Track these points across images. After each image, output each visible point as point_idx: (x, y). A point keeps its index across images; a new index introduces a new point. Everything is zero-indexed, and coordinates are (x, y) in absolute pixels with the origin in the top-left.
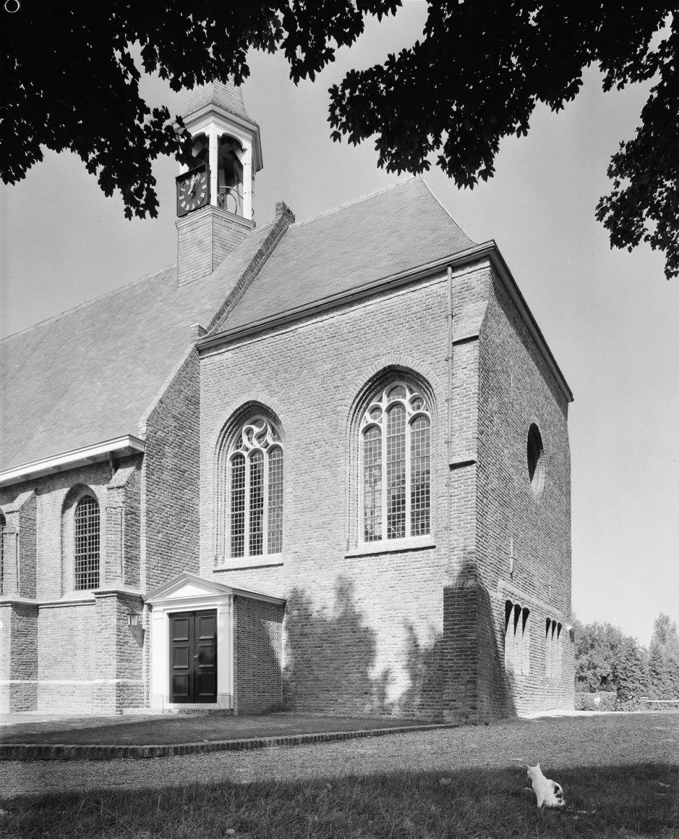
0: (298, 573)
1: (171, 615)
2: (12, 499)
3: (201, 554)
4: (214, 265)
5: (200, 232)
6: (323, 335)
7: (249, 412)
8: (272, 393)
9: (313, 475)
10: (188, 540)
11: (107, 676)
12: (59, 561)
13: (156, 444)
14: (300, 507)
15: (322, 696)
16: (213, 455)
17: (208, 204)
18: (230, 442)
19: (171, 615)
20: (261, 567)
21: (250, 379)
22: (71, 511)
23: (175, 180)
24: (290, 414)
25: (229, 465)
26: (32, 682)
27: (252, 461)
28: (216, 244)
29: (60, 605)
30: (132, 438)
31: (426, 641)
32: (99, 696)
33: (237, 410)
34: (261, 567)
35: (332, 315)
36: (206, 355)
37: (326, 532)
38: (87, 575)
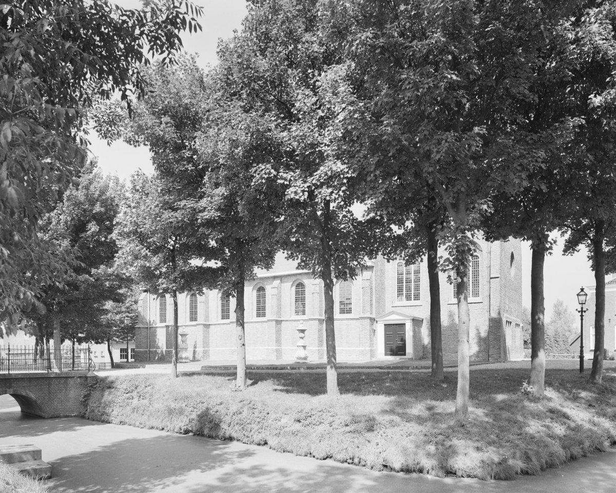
1: (385, 325)
19: (385, 325)
31: (483, 334)
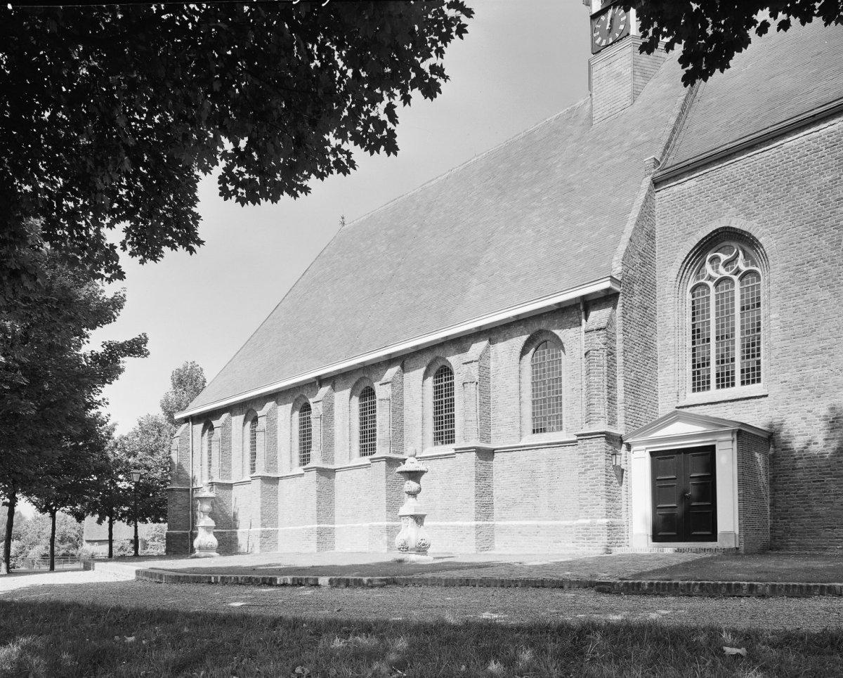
0: (788, 404)
2: (465, 350)
3: (659, 390)
4: (635, 95)
5: (617, 65)
6: (820, 146)
7: (715, 241)
8: (749, 216)
9: (807, 297)
10: (650, 378)
11: (594, 516)
12: (518, 407)
13: (627, 281)
14: (789, 332)
15: (823, 533)
16: (673, 288)
17: (628, 34)
18: (691, 273)
19: (652, 454)
20: (738, 400)
21: (720, 205)
22: (529, 356)
23: (589, 18)
24: (775, 236)
25: (689, 296)
26: (491, 523)
27: (717, 291)
28: (637, 73)
29: (519, 449)
30: (612, 279)
32: (586, 535)
33: (703, 239)
34: (738, 400)
35: (832, 122)
36: (664, 187)
37: (826, 357)
38: (444, 431)
